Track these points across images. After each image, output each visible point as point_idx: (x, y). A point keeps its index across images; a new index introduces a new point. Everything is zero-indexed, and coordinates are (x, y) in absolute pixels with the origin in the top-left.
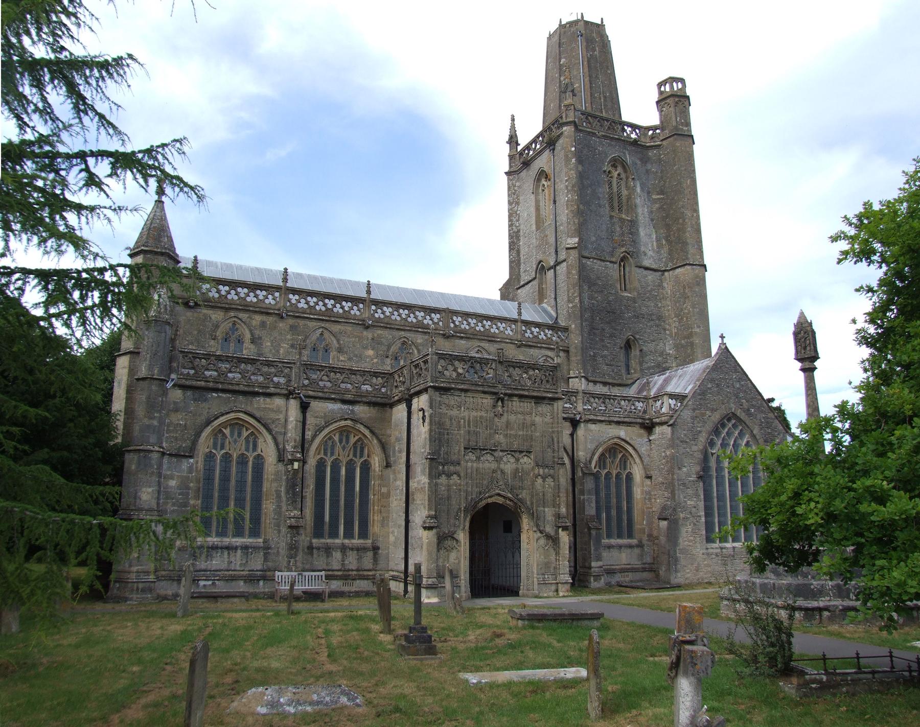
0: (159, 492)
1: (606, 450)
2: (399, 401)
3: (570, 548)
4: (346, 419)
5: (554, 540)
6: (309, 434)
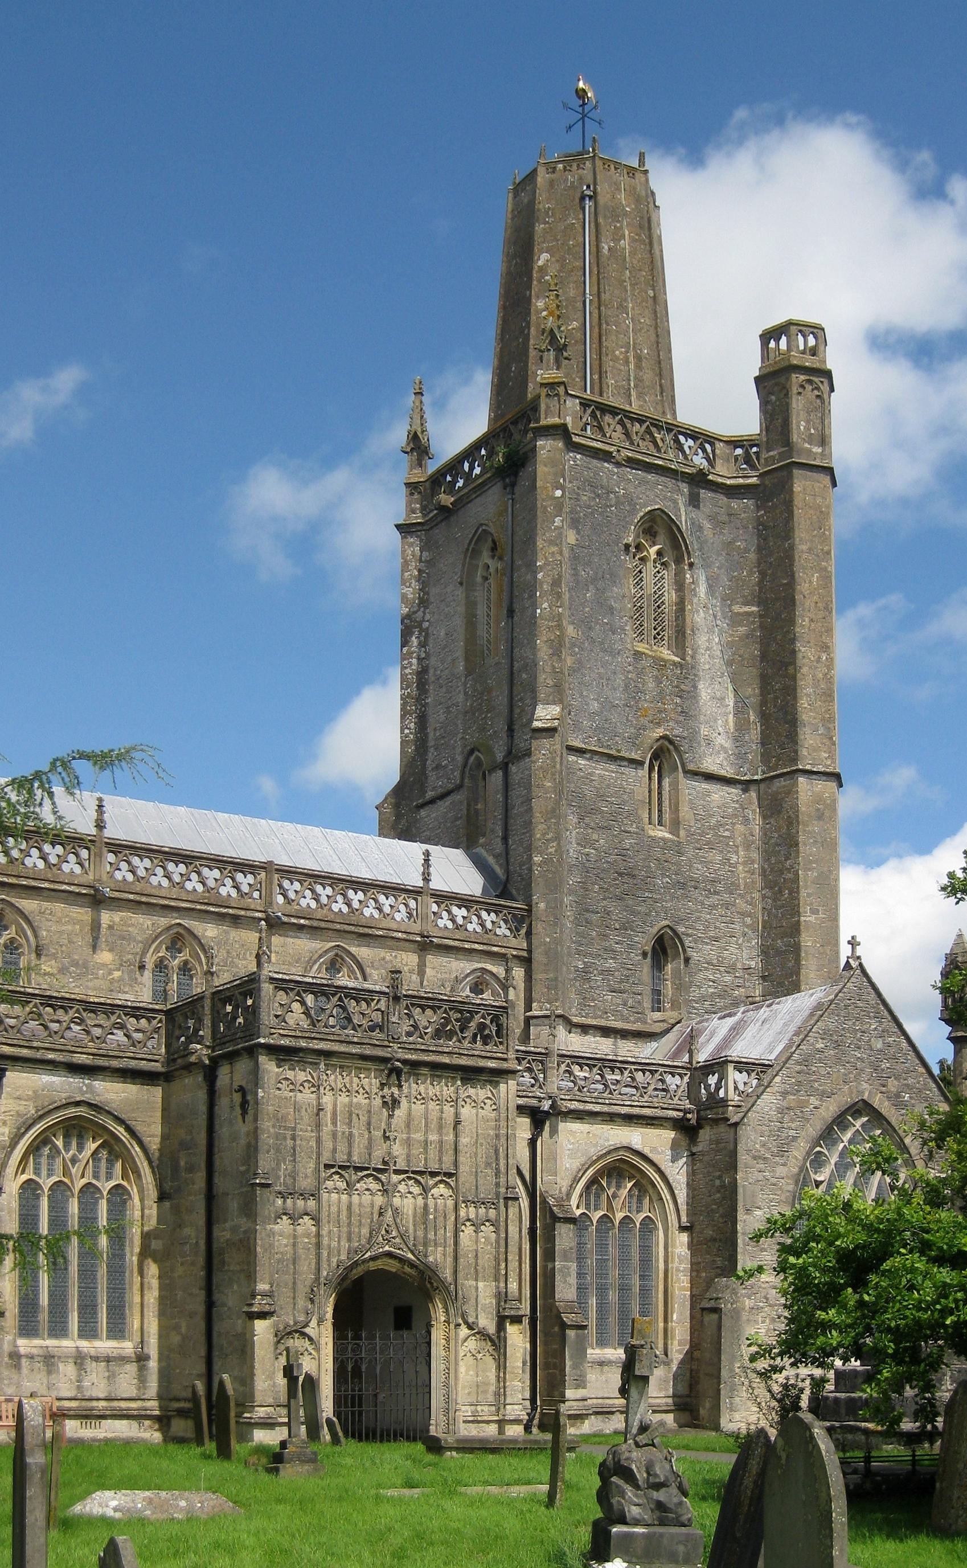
1: (600, 1173)
3: (524, 1363)
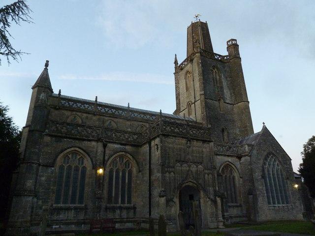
0: (36, 182)
2: (145, 144)
4: (122, 152)
5: (215, 202)
6: (106, 158)
